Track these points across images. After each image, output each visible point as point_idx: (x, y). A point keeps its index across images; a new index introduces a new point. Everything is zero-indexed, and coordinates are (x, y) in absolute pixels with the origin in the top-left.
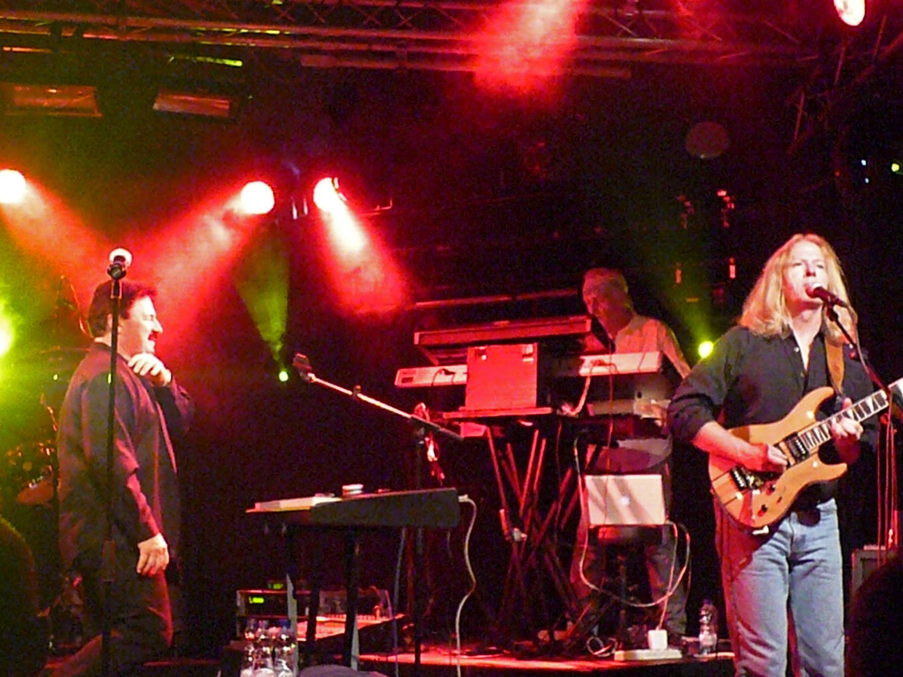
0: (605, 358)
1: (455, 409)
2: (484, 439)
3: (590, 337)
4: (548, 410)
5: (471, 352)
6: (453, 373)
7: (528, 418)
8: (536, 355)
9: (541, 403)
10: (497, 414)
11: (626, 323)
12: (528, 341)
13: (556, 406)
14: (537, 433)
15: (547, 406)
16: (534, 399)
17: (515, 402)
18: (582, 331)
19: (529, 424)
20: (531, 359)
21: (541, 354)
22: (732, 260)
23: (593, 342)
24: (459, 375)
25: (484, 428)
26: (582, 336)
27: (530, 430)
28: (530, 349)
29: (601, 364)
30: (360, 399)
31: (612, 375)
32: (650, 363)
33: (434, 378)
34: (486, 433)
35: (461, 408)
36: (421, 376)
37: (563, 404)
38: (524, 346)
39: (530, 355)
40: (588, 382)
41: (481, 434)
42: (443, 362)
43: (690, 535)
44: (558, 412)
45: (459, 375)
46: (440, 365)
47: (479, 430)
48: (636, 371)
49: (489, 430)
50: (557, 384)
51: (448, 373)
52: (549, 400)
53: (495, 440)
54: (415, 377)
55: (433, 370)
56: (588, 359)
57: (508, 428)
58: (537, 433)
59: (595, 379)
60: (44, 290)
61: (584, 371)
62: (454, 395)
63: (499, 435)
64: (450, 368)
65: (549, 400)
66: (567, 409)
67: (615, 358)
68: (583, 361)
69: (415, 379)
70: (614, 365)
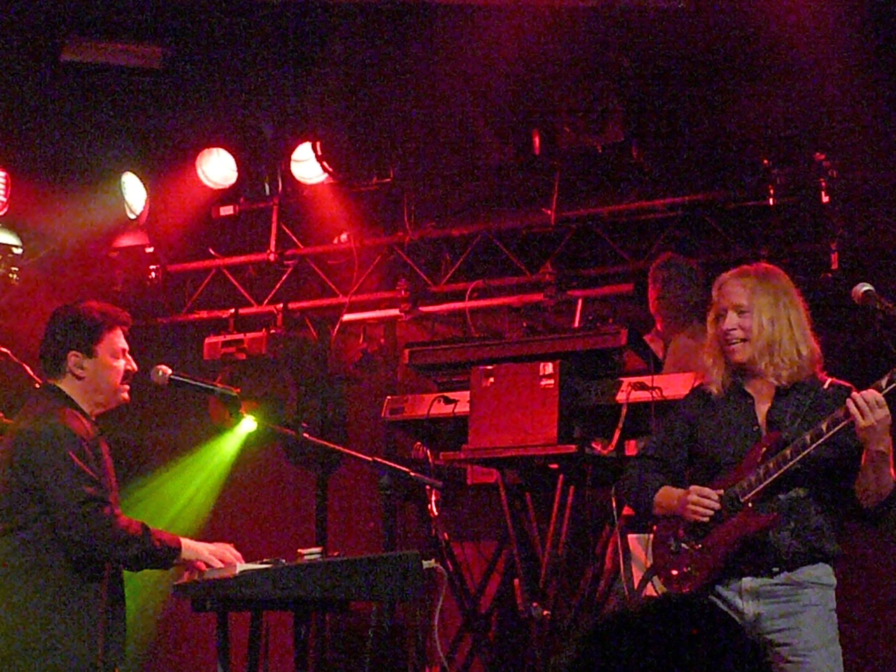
0: (646, 380)
2: (495, 487)
6: (455, 402)
9: (565, 436)
12: (546, 358)
13: (585, 441)
20: (552, 382)
21: (560, 375)
22: (833, 247)
23: (631, 359)
24: (462, 402)
26: (620, 350)
27: (554, 474)
28: (549, 368)
29: (642, 387)
30: (422, 312)
33: (429, 410)
35: (464, 446)
37: (594, 440)
39: (549, 377)
40: (624, 411)
44: (587, 450)
45: (462, 402)
47: (491, 474)
50: (586, 414)
51: (448, 401)
57: (531, 474)
59: (635, 407)
61: (621, 397)
64: (451, 395)
67: (658, 380)
70: (659, 389)
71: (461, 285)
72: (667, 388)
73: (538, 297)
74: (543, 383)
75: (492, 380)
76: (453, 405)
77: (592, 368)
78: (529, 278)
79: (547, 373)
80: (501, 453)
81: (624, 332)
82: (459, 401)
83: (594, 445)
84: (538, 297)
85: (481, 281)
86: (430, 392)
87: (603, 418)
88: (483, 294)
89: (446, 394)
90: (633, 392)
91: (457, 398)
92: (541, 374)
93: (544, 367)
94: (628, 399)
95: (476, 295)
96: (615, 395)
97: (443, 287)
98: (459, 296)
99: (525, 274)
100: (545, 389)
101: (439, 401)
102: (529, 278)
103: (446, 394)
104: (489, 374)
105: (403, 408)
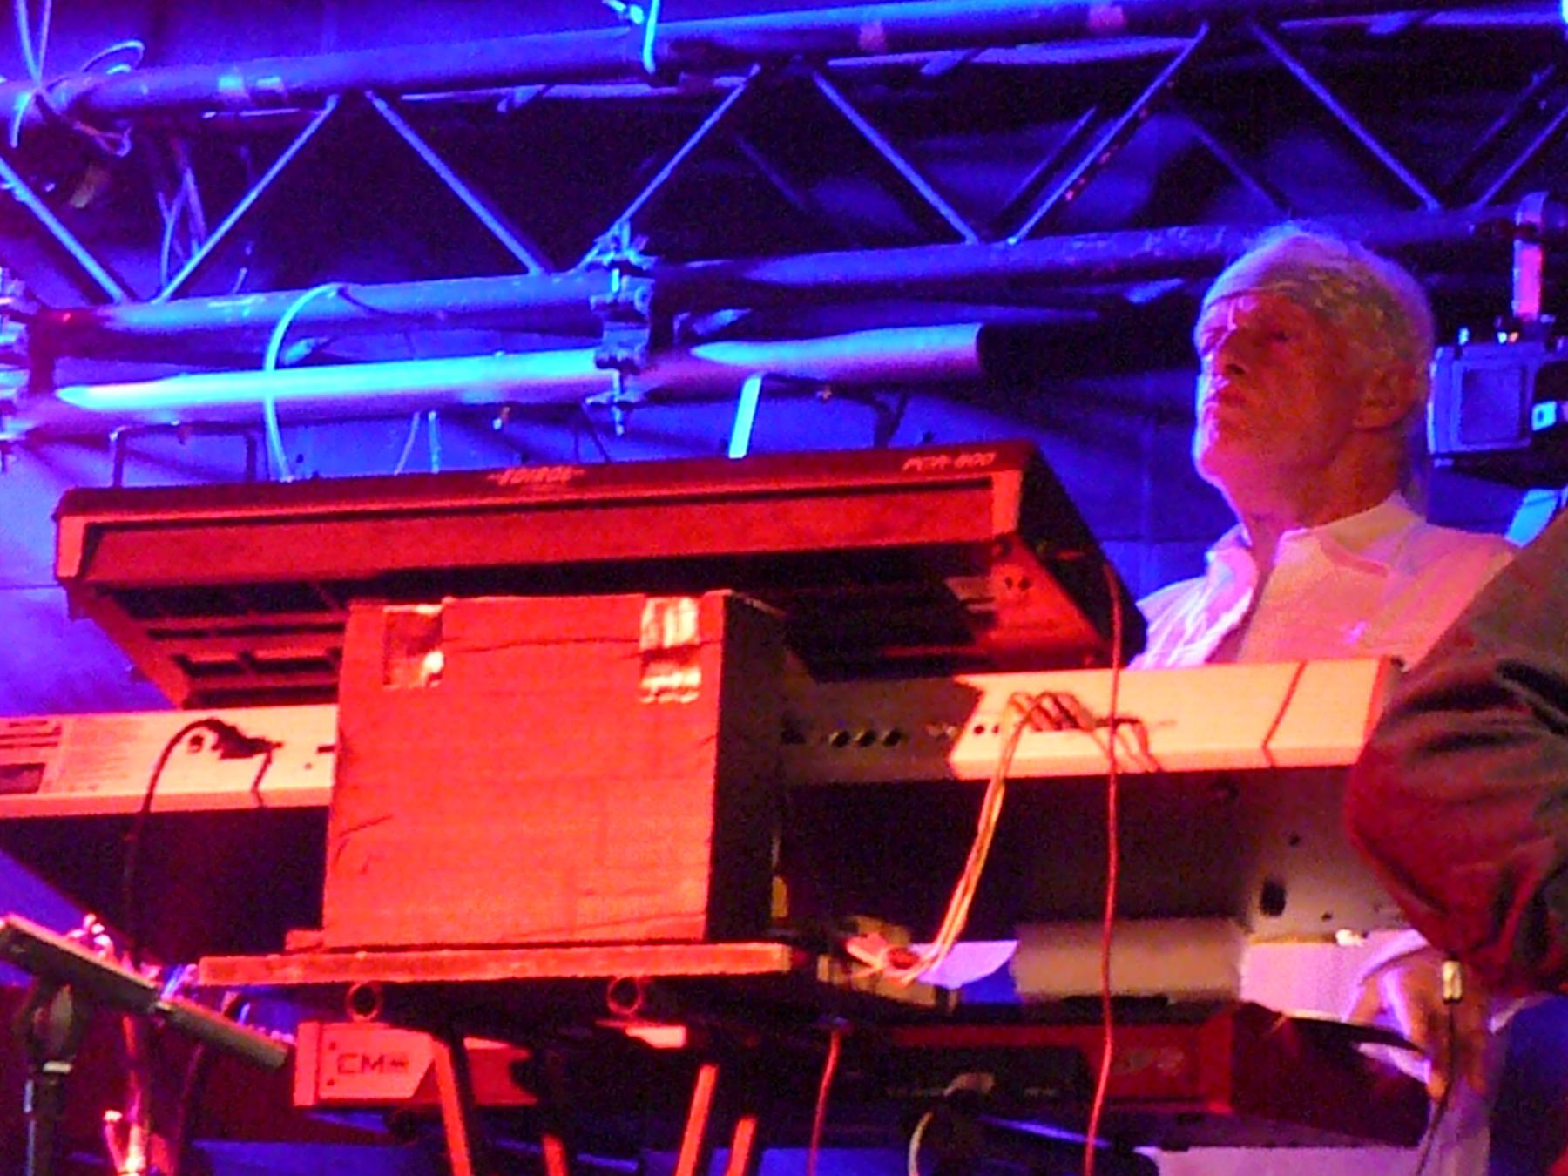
0: (1088, 687)
1: (270, 942)
3: (1015, 572)
4: (774, 956)
5: (363, 630)
7: (667, 998)
8: (715, 652)
9: (732, 912)
10: (492, 972)
11: (1386, 497)
13: (817, 935)
14: (706, 1078)
15: (760, 934)
16: (692, 892)
17: (586, 906)
18: (965, 534)
19: (668, 1036)
20: (692, 677)
21: (740, 653)
23: (1017, 596)
24: (297, 753)
25: (421, 1049)
26: (973, 558)
27: (673, 1070)
28: (681, 620)
29: (1066, 717)
31: (1128, 782)
32: (1325, 717)
34: (429, 1081)
35: (298, 938)
36: (86, 762)
37: (853, 929)
38: (54, 275)
39: (681, 655)
40: (534, 1148)
41: (402, 1086)
42: (213, 687)
43: (195, 173)
45: (297, 753)
46: (188, 706)
48: (1260, 762)
49: (444, 1052)
50: (824, 830)
51: (235, 745)
52: (779, 907)
53: (479, 1118)
54: (54, 760)
55: (161, 725)
56: (998, 691)
58: (706, 1078)
59: (1033, 796)
60: (1025, 584)
61: (973, 754)
62: (263, 869)
63: (502, 1092)
64: (251, 721)
65: (779, 907)
66: (872, 956)
68: (973, 697)
69: (51, 773)
71: (246, 306)
72: (1166, 724)
73: (570, 366)
74: (654, 682)
75: (434, 661)
76: (259, 759)
77: (849, 625)
78: (532, 284)
79: (670, 640)
80: (474, 964)
81: (1007, 489)
82: (279, 745)
83: (854, 949)
84: (570, 366)
85: (329, 290)
86: (158, 703)
87: (898, 845)
88: (328, 343)
89: (229, 716)
90: (1027, 732)
91: (273, 737)
92: (645, 643)
93: (660, 611)
94: (1007, 761)
95: (300, 349)
96: (947, 745)
97: (161, 313)
98: (235, 349)
99: (523, 270)
100: (665, 713)
101: (197, 741)
102: (532, 284)
103: (229, 716)
104: (430, 637)
105: (40, 767)
